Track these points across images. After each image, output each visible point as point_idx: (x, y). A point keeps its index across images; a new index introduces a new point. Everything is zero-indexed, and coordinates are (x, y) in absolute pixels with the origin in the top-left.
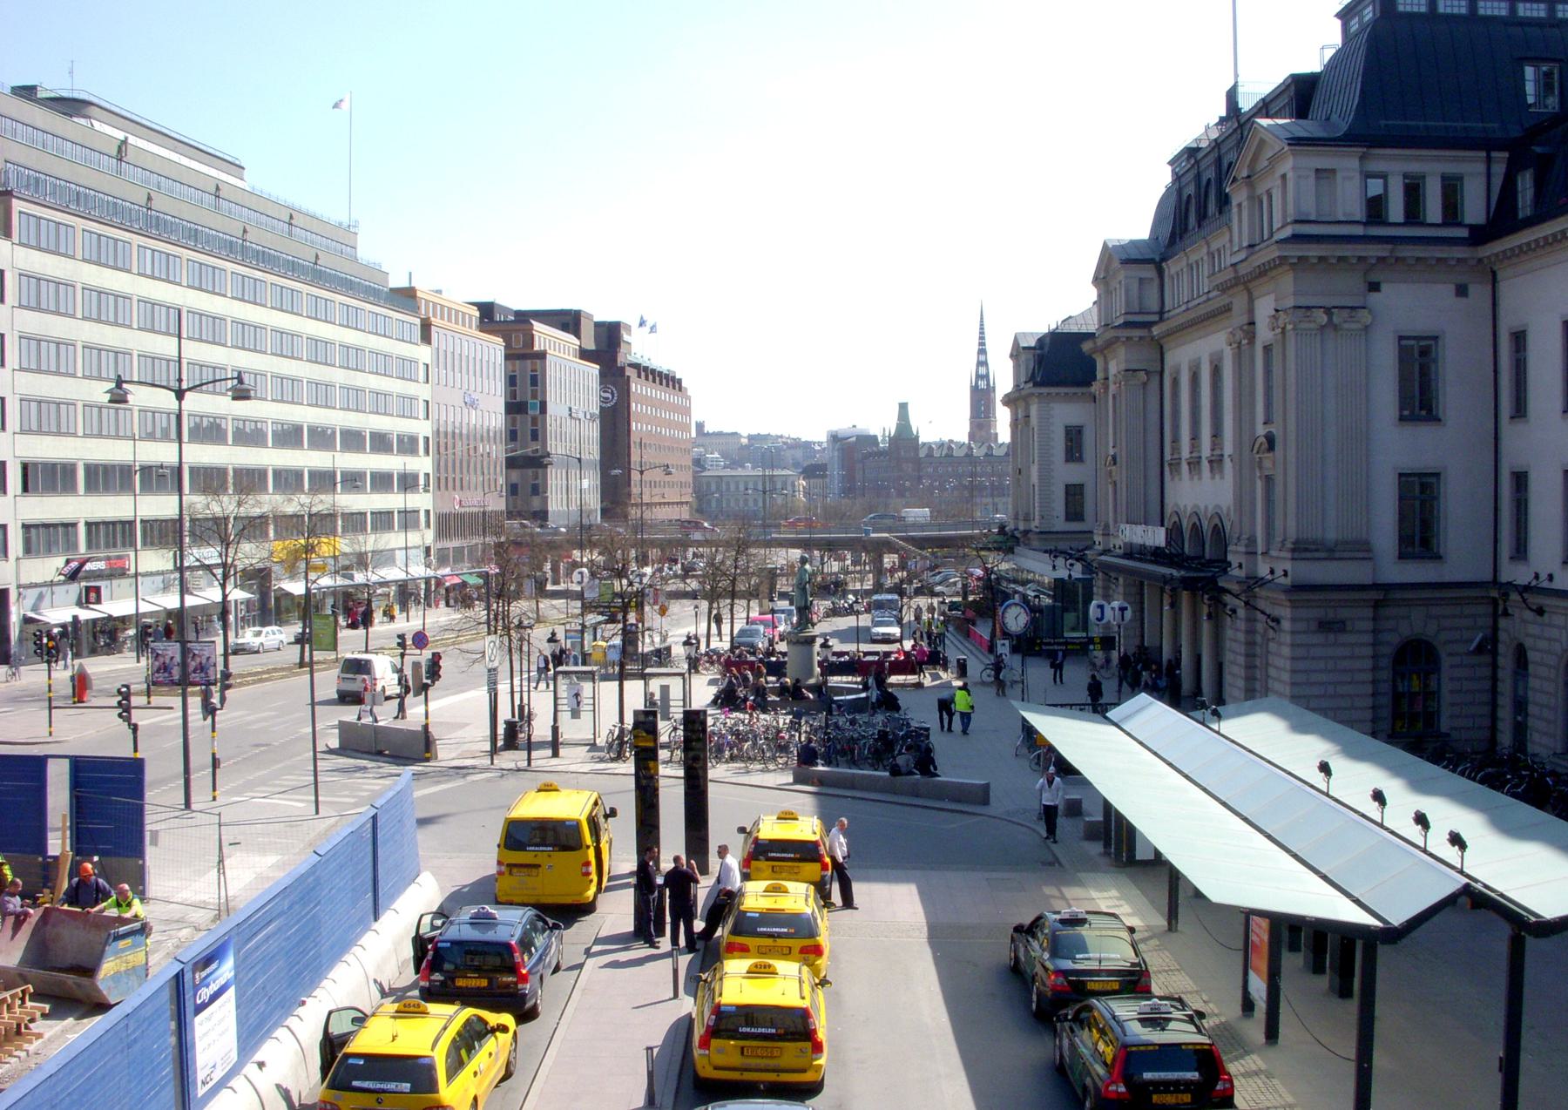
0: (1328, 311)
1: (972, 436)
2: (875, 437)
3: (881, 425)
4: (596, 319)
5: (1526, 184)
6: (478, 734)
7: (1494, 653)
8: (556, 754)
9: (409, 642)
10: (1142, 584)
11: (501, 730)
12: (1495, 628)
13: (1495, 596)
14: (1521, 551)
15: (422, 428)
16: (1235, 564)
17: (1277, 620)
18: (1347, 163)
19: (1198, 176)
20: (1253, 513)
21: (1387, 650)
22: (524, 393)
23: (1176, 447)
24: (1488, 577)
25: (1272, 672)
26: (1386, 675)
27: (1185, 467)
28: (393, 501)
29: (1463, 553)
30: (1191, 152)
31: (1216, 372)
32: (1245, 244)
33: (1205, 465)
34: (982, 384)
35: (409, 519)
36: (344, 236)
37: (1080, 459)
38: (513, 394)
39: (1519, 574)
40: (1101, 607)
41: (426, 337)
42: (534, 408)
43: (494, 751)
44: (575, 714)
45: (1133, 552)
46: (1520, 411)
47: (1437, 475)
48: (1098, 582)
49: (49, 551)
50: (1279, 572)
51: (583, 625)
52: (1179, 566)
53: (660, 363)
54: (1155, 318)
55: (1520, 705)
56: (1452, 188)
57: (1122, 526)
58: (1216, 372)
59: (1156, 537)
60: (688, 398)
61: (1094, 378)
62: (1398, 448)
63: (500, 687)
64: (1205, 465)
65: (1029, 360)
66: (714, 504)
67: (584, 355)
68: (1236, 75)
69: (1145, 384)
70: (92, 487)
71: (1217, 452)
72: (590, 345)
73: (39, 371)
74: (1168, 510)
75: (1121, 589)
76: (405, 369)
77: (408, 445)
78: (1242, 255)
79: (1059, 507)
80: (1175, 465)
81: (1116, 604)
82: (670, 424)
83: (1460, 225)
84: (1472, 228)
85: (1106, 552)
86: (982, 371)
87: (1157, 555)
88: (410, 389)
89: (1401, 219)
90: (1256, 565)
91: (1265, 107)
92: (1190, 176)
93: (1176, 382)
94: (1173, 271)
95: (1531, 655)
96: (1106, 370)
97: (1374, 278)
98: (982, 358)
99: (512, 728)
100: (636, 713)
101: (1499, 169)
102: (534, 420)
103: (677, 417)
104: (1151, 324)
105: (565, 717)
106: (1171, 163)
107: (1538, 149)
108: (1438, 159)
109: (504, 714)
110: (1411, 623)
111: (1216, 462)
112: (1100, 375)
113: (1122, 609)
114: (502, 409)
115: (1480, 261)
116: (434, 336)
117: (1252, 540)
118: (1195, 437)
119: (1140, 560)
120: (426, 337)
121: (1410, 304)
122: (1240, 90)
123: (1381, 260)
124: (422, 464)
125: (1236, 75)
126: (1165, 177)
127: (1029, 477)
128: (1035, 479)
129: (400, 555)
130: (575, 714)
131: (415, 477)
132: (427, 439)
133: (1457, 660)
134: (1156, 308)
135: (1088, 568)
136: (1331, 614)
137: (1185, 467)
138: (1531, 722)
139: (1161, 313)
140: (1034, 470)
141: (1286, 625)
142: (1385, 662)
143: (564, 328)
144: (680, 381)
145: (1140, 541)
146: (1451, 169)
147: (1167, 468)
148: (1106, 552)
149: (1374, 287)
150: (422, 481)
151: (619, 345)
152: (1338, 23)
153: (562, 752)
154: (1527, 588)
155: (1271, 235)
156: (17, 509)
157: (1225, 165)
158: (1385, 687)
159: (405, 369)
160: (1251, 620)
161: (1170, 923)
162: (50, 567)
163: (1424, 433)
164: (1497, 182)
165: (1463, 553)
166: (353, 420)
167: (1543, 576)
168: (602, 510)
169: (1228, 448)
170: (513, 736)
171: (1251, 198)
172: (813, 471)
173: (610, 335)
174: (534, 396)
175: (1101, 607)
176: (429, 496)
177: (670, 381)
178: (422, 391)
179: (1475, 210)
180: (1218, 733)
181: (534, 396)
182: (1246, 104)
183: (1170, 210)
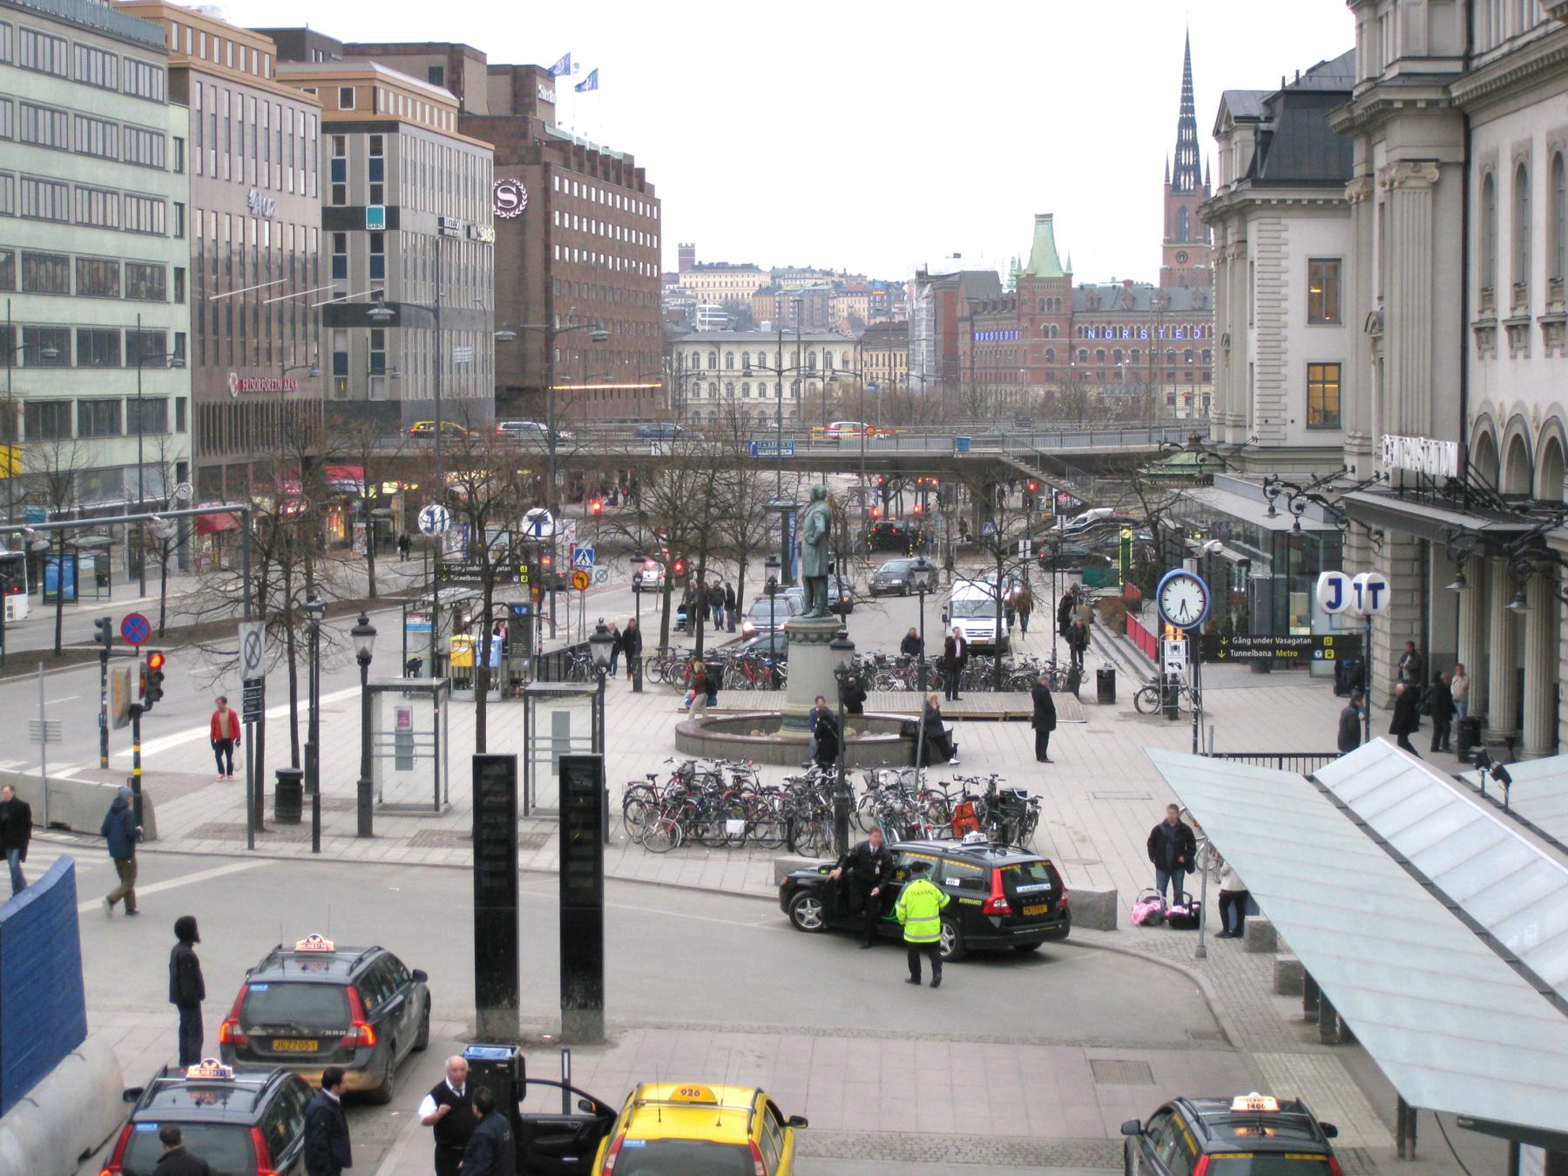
1: (1166, 274)
2: (993, 276)
4: (489, 62)
9: (116, 631)
10: (1424, 545)
11: (270, 785)
15: (176, 254)
22: (358, 192)
23: (1488, 294)
27: (1502, 335)
28: (117, 382)
34: (1187, 182)
35: (147, 416)
37: (336, 355)
38: (339, 193)
40: (1336, 583)
41: (178, 89)
43: (256, 824)
44: (405, 760)
45: (1416, 487)
48: (1352, 538)
52: (1483, 510)
54: (1457, 67)
59: (1442, 459)
60: (657, 203)
63: (269, 714)
65: (1245, 137)
67: (468, 124)
69: (1436, 186)
71: (1520, 312)
72: (478, 104)
75: (1387, 551)
76: (138, 147)
79: (1295, 405)
80: (1486, 331)
81: (1364, 578)
82: (621, 249)
85: (1361, 486)
87: (1455, 492)
88: (151, 182)
93: (1489, 183)
96: (1369, 160)
98: (1187, 135)
99: (288, 782)
100: (279, 775)
102: (377, 241)
104: (1454, 77)
105: (386, 767)
112: (1359, 171)
113: (1375, 588)
114: (317, 221)
116: (195, 89)
118: (1521, 289)
119: (1417, 500)
120: (178, 89)
124: (173, 318)
128: (1253, 354)
129: (129, 478)
130: (405, 760)
131: (159, 338)
132: (179, 272)
134: (1458, 49)
135: (1332, 513)
137: (1502, 335)
139: (1468, 57)
140: (1253, 335)
143: (435, 76)
144: (641, 172)
148: (1361, 486)
150: (171, 347)
151: (531, 107)
153: (379, 824)
159: (138, 147)
161: (1401, 1144)
166: (47, 238)
168: (498, 398)
173: (523, 84)
174: (376, 196)
175: (1336, 583)
176: (186, 374)
177: (623, 174)
178: (175, 188)
180: (1505, 809)
181: (376, 196)
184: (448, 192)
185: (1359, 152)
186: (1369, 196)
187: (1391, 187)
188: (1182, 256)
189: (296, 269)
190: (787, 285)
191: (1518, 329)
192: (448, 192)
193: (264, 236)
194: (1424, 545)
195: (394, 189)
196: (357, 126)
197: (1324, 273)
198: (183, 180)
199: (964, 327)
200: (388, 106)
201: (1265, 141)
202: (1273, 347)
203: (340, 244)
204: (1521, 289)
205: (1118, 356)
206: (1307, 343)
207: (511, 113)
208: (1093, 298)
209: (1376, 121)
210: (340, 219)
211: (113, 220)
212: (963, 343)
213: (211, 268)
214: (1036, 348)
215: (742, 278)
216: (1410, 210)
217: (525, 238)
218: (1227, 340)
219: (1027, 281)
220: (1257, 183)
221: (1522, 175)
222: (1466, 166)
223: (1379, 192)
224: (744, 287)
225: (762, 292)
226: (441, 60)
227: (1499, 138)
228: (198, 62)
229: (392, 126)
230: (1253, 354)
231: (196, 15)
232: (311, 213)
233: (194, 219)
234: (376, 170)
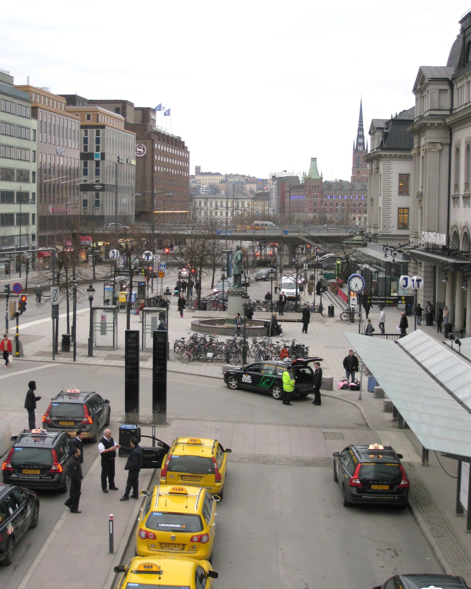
1: (353, 178)
2: (297, 178)
3: (299, 169)
4: (135, 106)
6: (47, 343)
8: (90, 354)
10: (435, 267)
11: (60, 339)
15: (33, 167)
22: (92, 148)
23: (457, 186)
27: (461, 200)
37: (407, 194)
38: (86, 148)
40: (406, 279)
41: (34, 114)
42: (97, 156)
43: (55, 352)
44: (103, 332)
45: (432, 248)
48: (412, 265)
51: (114, 281)
52: (454, 256)
54: (448, 113)
57: (423, 233)
59: (441, 240)
61: (412, 148)
66: (203, 214)
67: (128, 126)
69: (440, 151)
72: (131, 120)
76: (21, 133)
77: (23, 176)
80: (456, 198)
85: (415, 248)
86: (361, 141)
87: (445, 250)
88: (25, 144)
93: (458, 150)
94: (459, 85)
96: (419, 142)
98: (361, 133)
99: (66, 339)
100: (63, 336)
102: (98, 163)
103: (180, 163)
106: (461, 22)
109: (63, 330)
112: (416, 146)
116: (40, 114)
119: (433, 253)
120: (34, 114)
124: (31, 188)
126: (457, 29)
127: (378, 203)
128: (381, 204)
129: (17, 239)
130: (103, 332)
132: (34, 173)
134: (448, 107)
135: (405, 256)
137: (461, 200)
143: (117, 111)
145: (433, 242)
147: (451, 200)
148: (415, 248)
153: (95, 352)
159: (21, 133)
161: (423, 461)
168: (136, 215)
170: (66, 344)
172: (262, 196)
173: (146, 114)
174: (98, 149)
175: (406, 279)
176: (35, 206)
178: (33, 146)
180: (459, 353)
181: (98, 149)
184: (121, 149)
186: (419, 154)
189: (71, 173)
190: (230, 180)
192: (121, 149)
193: (61, 162)
194: (435, 267)
195: (103, 147)
197: (404, 179)
198: (35, 143)
199: (287, 194)
200: (102, 120)
201: (386, 136)
202: (387, 202)
203: (86, 165)
205: (337, 204)
206: (398, 201)
207: (141, 122)
208: (329, 185)
209: (421, 130)
210: (86, 157)
212: (287, 200)
213: (44, 172)
214: (310, 201)
215: (216, 177)
216: (432, 159)
217: (145, 163)
218: (372, 200)
222: (450, 145)
223: (422, 153)
224: (216, 180)
225: (222, 182)
226: (119, 106)
228: (39, 105)
229: (103, 127)
230: (381, 204)
234: (98, 141)
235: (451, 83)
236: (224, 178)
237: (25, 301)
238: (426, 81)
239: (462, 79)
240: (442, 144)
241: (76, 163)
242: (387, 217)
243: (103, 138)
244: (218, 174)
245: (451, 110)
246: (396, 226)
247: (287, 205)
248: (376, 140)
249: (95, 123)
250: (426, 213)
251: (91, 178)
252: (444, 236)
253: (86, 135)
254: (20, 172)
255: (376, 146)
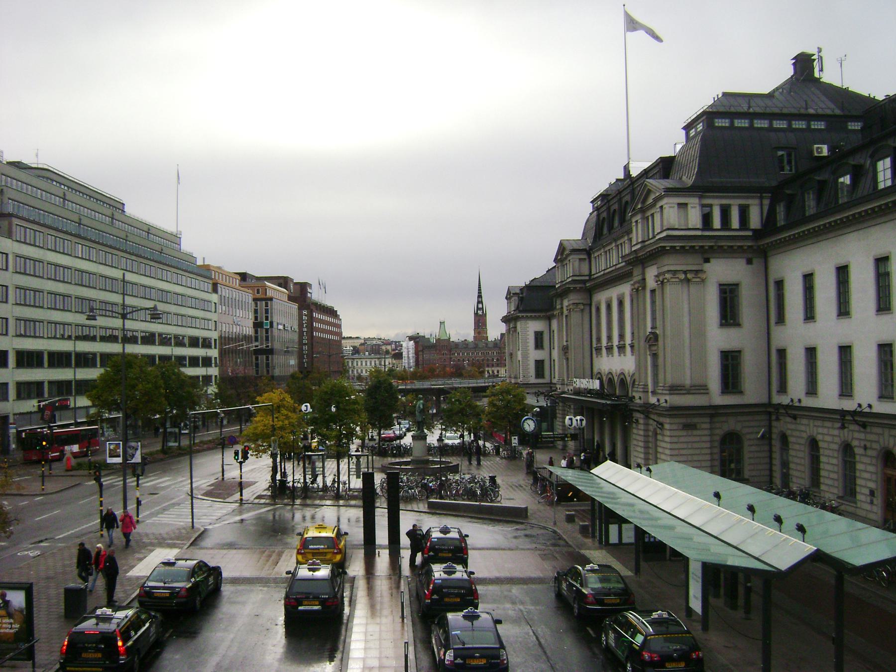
0: (685, 272)
5: (781, 210)
7: (770, 439)
12: (770, 427)
13: (770, 411)
14: (783, 388)
15: (214, 335)
16: (637, 397)
17: (662, 424)
18: (693, 202)
19: (609, 208)
20: (646, 374)
21: (717, 438)
22: (262, 316)
23: (599, 340)
24: (765, 400)
25: (660, 450)
26: (717, 450)
27: (604, 351)
29: (753, 390)
30: (604, 196)
31: (621, 303)
32: (640, 240)
33: (616, 349)
34: (480, 312)
36: (175, 239)
37: (738, 325)
38: (256, 318)
39: (785, 400)
40: (571, 419)
41: (215, 290)
45: (578, 392)
46: (781, 319)
47: (739, 352)
49: (29, 397)
50: (662, 401)
53: (328, 302)
54: (587, 278)
55: (785, 464)
56: (744, 212)
58: (621, 303)
59: (596, 385)
62: (719, 339)
64: (616, 349)
65: (515, 299)
67: (291, 298)
68: (629, 158)
69: (582, 310)
70: (51, 365)
71: (622, 343)
73: (25, 305)
74: (595, 370)
76: (204, 305)
77: (206, 344)
78: (639, 246)
80: (599, 350)
82: (331, 333)
83: (748, 229)
84: (754, 231)
89: (719, 227)
90: (648, 398)
91: (646, 173)
92: (605, 208)
93: (598, 309)
95: (791, 439)
96: (562, 304)
97: (706, 256)
101: (766, 202)
102: (267, 330)
103: (335, 329)
107: (788, 192)
108: (717, 197)
110: (731, 424)
111: (621, 348)
112: (558, 307)
113: (581, 420)
115: (759, 247)
116: (219, 289)
117: (646, 385)
118: (610, 338)
119: (579, 395)
120: (215, 290)
121: (722, 270)
122: (631, 165)
123: (711, 247)
124: (214, 353)
125: (629, 158)
126: (590, 208)
128: (520, 357)
132: (215, 340)
133: (752, 442)
134: (587, 273)
136: (689, 421)
137: (604, 351)
138: (791, 472)
141: (667, 426)
142: (716, 444)
143: (280, 285)
146: (725, 202)
147: (594, 352)
149: (707, 260)
152: (684, 132)
154: (787, 407)
155: (654, 237)
156: (12, 375)
157: (624, 202)
158: (717, 457)
160: (646, 424)
162: (31, 405)
163: (732, 332)
164: (766, 209)
165: (753, 390)
167: (796, 400)
169: (628, 340)
171: (642, 218)
173: (303, 287)
174: (267, 319)
175: (571, 419)
178: (214, 317)
179: (755, 221)
181: (267, 319)
182: (634, 173)
183: (593, 224)
184: (285, 317)
185: (558, 302)
186: (562, 313)
187: (569, 310)
188: (479, 333)
189: (247, 338)
190: (369, 343)
191: (621, 348)
192: (285, 317)
193: (236, 330)
194: (582, 407)
195: (272, 317)
196: (263, 300)
197: (539, 336)
198: (216, 314)
199: (420, 353)
200: (270, 293)
201: (521, 300)
202: (525, 356)
203: (256, 332)
204: (610, 338)
205: (464, 361)
206: (535, 355)
207: (300, 294)
208: (456, 345)
209: (564, 292)
210: (257, 325)
211: (184, 324)
212: (420, 358)
213: (224, 339)
214: (441, 358)
215: (355, 341)
216: (575, 318)
217: (307, 329)
218: (511, 354)
219: (438, 340)
220: (520, 312)
221: (609, 307)
222: (590, 305)
223: (565, 312)
224: (357, 343)
225: (361, 344)
226: (282, 281)
227: (601, 297)
228: (220, 281)
229: (271, 299)
230: (520, 357)
231: (219, 268)
232: (250, 323)
233: (219, 325)
234: (267, 311)
235: (588, 252)
236: (363, 341)
237: (541, 421)
238: (567, 252)
239: (600, 249)
240: (584, 304)
241: (249, 330)
242: (526, 369)
243: (272, 309)
244: (357, 338)
245: (590, 275)
246: (534, 376)
247: (421, 362)
248: (513, 304)
249: (263, 296)
250: (572, 363)
251: (262, 344)
252: (597, 382)
253: (64, 331)
254: (205, 339)
255: (513, 309)
